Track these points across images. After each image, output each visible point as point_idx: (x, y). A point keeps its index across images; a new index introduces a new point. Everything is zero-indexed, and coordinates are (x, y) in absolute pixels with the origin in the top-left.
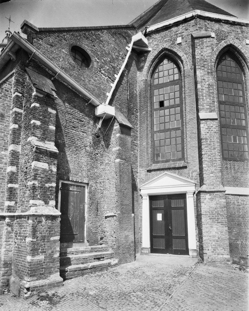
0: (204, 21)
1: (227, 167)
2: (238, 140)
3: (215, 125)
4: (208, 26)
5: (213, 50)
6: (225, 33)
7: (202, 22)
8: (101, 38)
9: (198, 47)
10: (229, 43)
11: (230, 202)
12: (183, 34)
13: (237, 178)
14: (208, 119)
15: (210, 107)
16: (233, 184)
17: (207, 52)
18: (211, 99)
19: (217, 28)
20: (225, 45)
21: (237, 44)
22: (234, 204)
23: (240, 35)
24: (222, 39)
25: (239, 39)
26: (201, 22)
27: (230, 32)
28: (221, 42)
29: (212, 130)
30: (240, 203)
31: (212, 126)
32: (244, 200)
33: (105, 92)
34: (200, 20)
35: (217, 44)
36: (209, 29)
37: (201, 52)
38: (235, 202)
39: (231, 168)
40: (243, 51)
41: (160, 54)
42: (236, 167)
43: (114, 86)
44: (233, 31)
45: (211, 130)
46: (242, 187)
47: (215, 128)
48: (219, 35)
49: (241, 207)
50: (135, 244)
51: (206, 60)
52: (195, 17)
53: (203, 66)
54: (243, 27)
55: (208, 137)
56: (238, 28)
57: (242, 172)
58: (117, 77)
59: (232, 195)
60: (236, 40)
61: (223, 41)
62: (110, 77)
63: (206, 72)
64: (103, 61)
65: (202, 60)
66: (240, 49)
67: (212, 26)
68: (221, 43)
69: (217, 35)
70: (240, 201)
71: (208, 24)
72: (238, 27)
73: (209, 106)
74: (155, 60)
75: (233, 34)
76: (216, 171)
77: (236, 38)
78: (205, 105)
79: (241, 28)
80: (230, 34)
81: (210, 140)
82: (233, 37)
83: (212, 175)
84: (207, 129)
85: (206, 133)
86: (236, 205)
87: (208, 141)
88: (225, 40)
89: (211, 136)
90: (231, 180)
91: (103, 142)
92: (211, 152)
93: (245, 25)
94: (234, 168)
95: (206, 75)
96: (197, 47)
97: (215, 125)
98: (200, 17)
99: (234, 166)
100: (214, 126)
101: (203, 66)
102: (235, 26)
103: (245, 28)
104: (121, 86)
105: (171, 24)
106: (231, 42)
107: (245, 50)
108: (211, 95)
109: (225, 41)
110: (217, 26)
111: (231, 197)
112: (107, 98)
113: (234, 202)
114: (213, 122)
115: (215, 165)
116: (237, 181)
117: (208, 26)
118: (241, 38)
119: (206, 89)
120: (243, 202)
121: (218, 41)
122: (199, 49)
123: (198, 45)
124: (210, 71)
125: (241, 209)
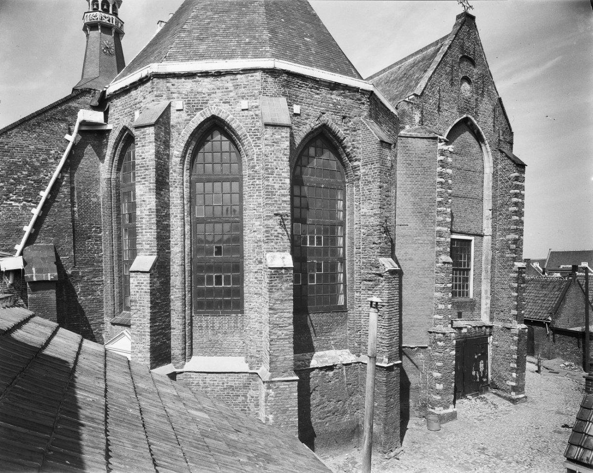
0: (165, 81)
1: (201, 326)
2: (310, 241)
3: (145, 280)
4: (173, 89)
5: (179, 134)
6: (204, 96)
7: (161, 83)
8: (6, 147)
9: (139, 143)
10: (209, 115)
11: (193, 383)
12: (142, 104)
13: (216, 343)
14: (138, 272)
15: (150, 246)
16: (209, 351)
17: (149, 153)
18: (152, 233)
19: (189, 90)
20: (202, 119)
21: (224, 112)
22: (198, 385)
23: (232, 94)
24: (197, 110)
25: (229, 102)
26: (160, 86)
27: (212, 91)
28: (195, 115)
29: (142, 289)
30: (208, 383)
31: (142, 281)
32: (215, 379)
33: (20, 227)
34: (158, 81)
35: (187, 121)
36: (173, 95)
37: (143, 153)
38: (201, 382)
39: (207, 327)
40: (234, 126)
41: (123, 135)
42: (217, 325)
43: (36, 211)
44: (218, 89)
45: (141, 288)
46: (223, 355)
47: (146, 286)
48: (191, 102)
49: (209, 389)
50: (106, 415)
51: (148, 166)
52: (150, 77)
53: (144, 178)
54: (239, 76)
55: (137, 299)
56: (229, 80)
57: (225, 333)
58: (44, 194)
59: (195, 372)
60: (223, 105)
61: (198, 113)
62: (30, 199)
63: (148, 188)
64: (13, 181)
65: (143, 167)
66: (228, 122)
67: (179, 87)
68: (195, 117)
69: (188, 103)
70: (208, 381)
71: (173, 85)
72: (228, 78)
73: (149, 246)
74: (118, 144)
75: (219, 94)
76: (144, 350)
77: (223, 103)
78: (144, 243)
79: (233, 80)
80: (213, 95)
81: (140, 303)
82: (217, 100)
83: (140, 355)
84: (137, 286)
85: (136, 293)
86: (201, 387)
87: (138, 305)
88: (202, 109)
89: (141, 298)
90: (206, 346)
91: (22, 301)
92: (140, 322)
93: (241, 72)
94: (213, 327)
95: (146, 194)
96: (137, 144)
97: (145, 280)
98: (158, 76)
99: (214, 323)
100: (145, 283)
101: (144, 178)
102: (223, 78)
103: (241, 79)
104: (56, 204)
105: (128, 86)
106: (214, 112)
107: (238, 122)
108: (152, 227)
109: (202, 111)
110: (187, 85)
111: (194, 375)
112: (24, 234)
113: (198, 383)
114: (143, 276)
115: (144, 341)
116: (215, 347)
117: (173, 89)
118: (232, 99)
119: (146, 217)
120: (212, 382)
121: (189, 115)
122: (140, 146)
123: (139, 139)
124: (152, 187)
125: (208, 393)
